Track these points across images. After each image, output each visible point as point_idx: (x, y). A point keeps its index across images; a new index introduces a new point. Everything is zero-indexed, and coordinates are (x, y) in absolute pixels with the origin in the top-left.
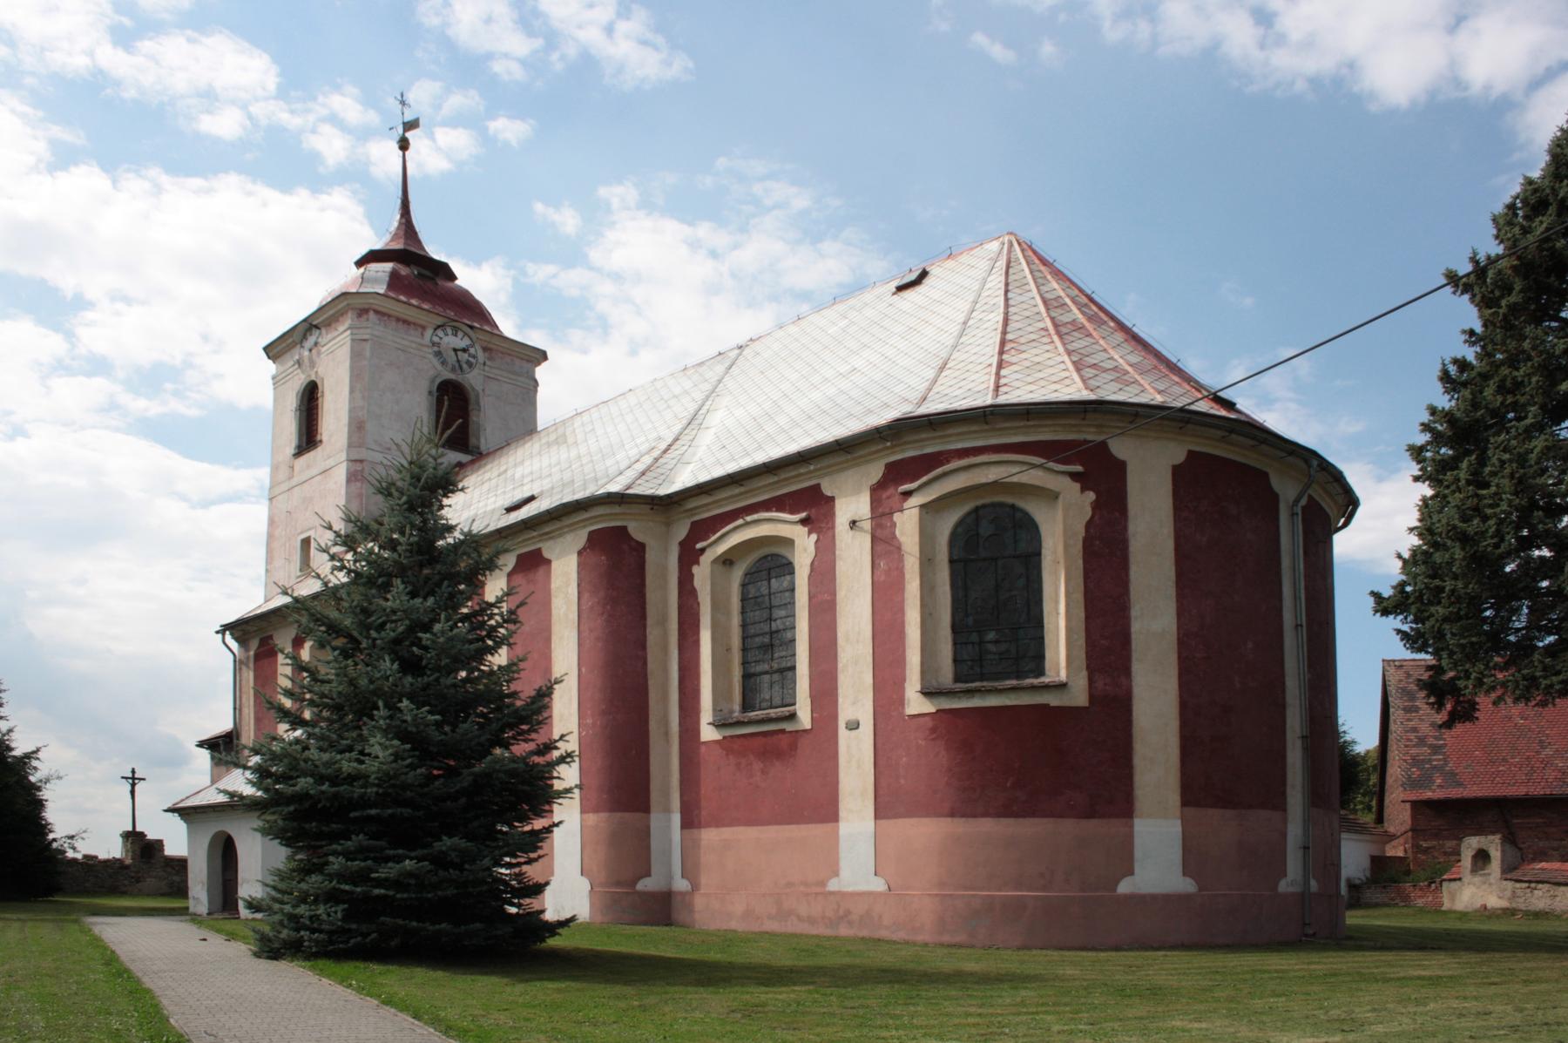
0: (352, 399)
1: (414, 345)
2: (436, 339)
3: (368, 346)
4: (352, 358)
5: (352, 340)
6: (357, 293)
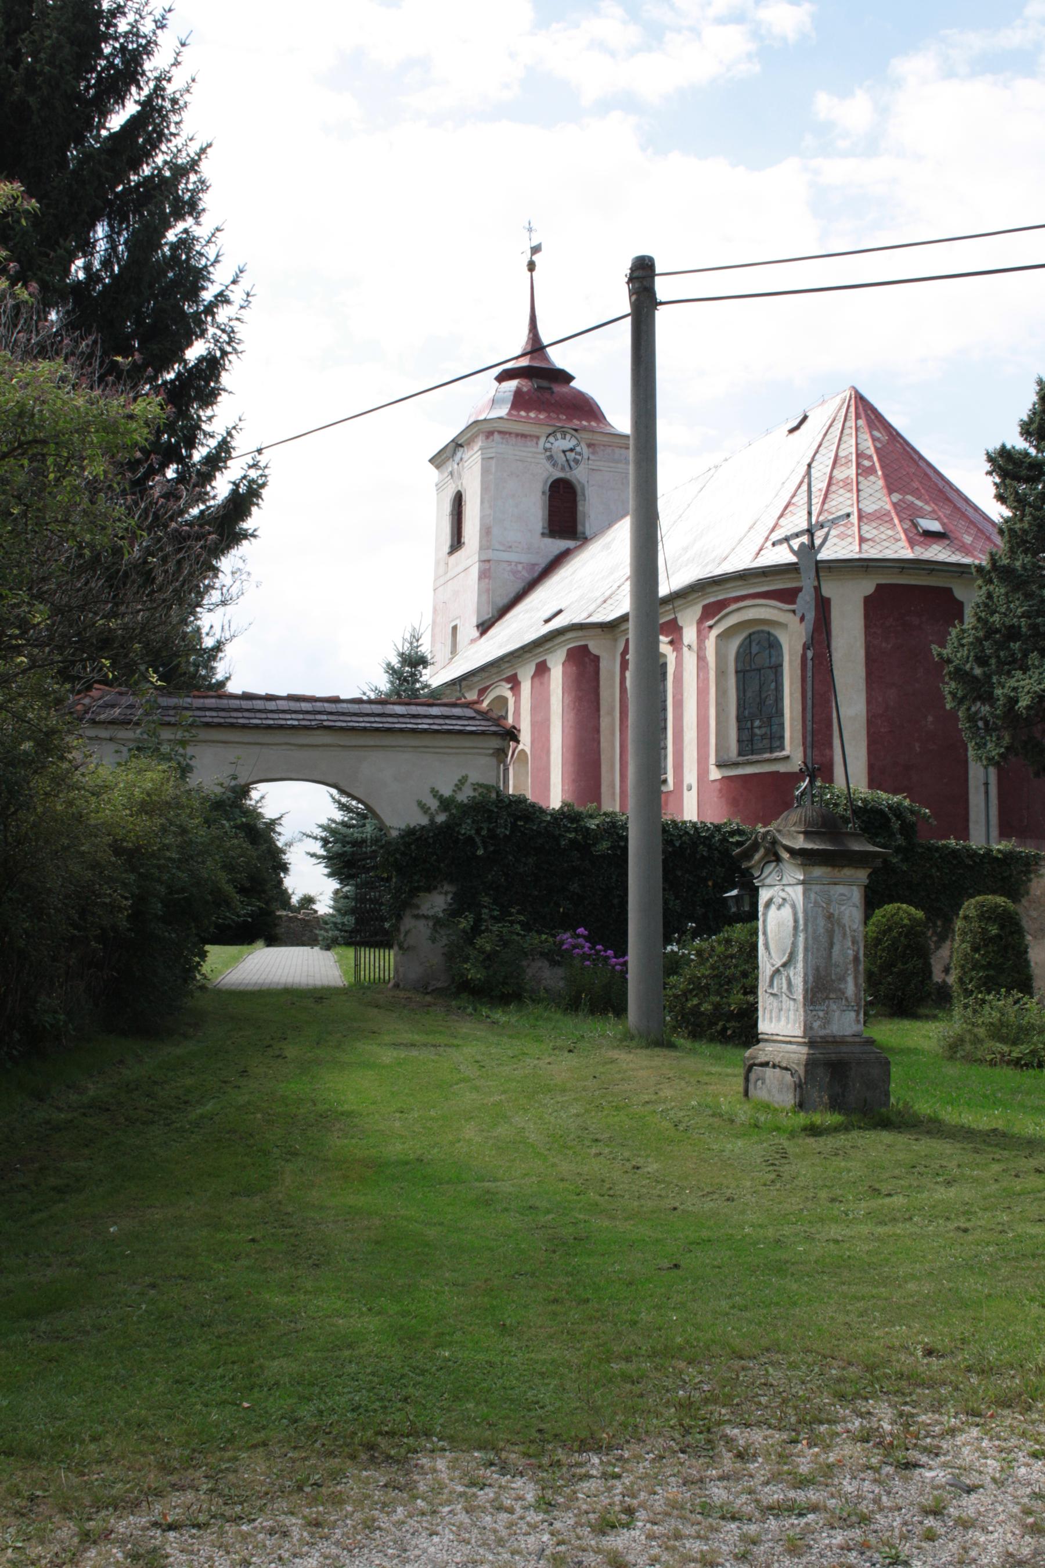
0: (482, 509)
1: (530, 455)
2: (548, 445)
3: (493, 462)
4: (482, 474)
5: (483, 459)
6: (485, 420)
